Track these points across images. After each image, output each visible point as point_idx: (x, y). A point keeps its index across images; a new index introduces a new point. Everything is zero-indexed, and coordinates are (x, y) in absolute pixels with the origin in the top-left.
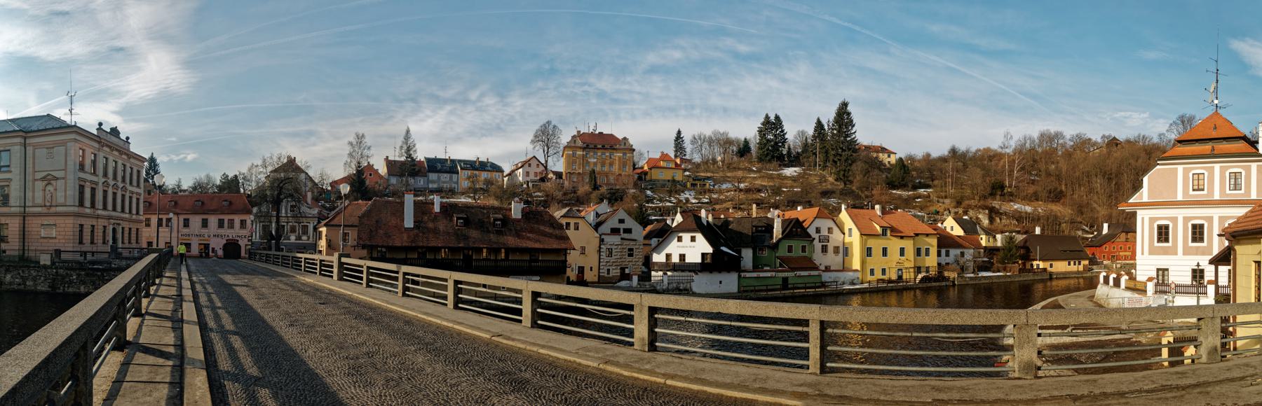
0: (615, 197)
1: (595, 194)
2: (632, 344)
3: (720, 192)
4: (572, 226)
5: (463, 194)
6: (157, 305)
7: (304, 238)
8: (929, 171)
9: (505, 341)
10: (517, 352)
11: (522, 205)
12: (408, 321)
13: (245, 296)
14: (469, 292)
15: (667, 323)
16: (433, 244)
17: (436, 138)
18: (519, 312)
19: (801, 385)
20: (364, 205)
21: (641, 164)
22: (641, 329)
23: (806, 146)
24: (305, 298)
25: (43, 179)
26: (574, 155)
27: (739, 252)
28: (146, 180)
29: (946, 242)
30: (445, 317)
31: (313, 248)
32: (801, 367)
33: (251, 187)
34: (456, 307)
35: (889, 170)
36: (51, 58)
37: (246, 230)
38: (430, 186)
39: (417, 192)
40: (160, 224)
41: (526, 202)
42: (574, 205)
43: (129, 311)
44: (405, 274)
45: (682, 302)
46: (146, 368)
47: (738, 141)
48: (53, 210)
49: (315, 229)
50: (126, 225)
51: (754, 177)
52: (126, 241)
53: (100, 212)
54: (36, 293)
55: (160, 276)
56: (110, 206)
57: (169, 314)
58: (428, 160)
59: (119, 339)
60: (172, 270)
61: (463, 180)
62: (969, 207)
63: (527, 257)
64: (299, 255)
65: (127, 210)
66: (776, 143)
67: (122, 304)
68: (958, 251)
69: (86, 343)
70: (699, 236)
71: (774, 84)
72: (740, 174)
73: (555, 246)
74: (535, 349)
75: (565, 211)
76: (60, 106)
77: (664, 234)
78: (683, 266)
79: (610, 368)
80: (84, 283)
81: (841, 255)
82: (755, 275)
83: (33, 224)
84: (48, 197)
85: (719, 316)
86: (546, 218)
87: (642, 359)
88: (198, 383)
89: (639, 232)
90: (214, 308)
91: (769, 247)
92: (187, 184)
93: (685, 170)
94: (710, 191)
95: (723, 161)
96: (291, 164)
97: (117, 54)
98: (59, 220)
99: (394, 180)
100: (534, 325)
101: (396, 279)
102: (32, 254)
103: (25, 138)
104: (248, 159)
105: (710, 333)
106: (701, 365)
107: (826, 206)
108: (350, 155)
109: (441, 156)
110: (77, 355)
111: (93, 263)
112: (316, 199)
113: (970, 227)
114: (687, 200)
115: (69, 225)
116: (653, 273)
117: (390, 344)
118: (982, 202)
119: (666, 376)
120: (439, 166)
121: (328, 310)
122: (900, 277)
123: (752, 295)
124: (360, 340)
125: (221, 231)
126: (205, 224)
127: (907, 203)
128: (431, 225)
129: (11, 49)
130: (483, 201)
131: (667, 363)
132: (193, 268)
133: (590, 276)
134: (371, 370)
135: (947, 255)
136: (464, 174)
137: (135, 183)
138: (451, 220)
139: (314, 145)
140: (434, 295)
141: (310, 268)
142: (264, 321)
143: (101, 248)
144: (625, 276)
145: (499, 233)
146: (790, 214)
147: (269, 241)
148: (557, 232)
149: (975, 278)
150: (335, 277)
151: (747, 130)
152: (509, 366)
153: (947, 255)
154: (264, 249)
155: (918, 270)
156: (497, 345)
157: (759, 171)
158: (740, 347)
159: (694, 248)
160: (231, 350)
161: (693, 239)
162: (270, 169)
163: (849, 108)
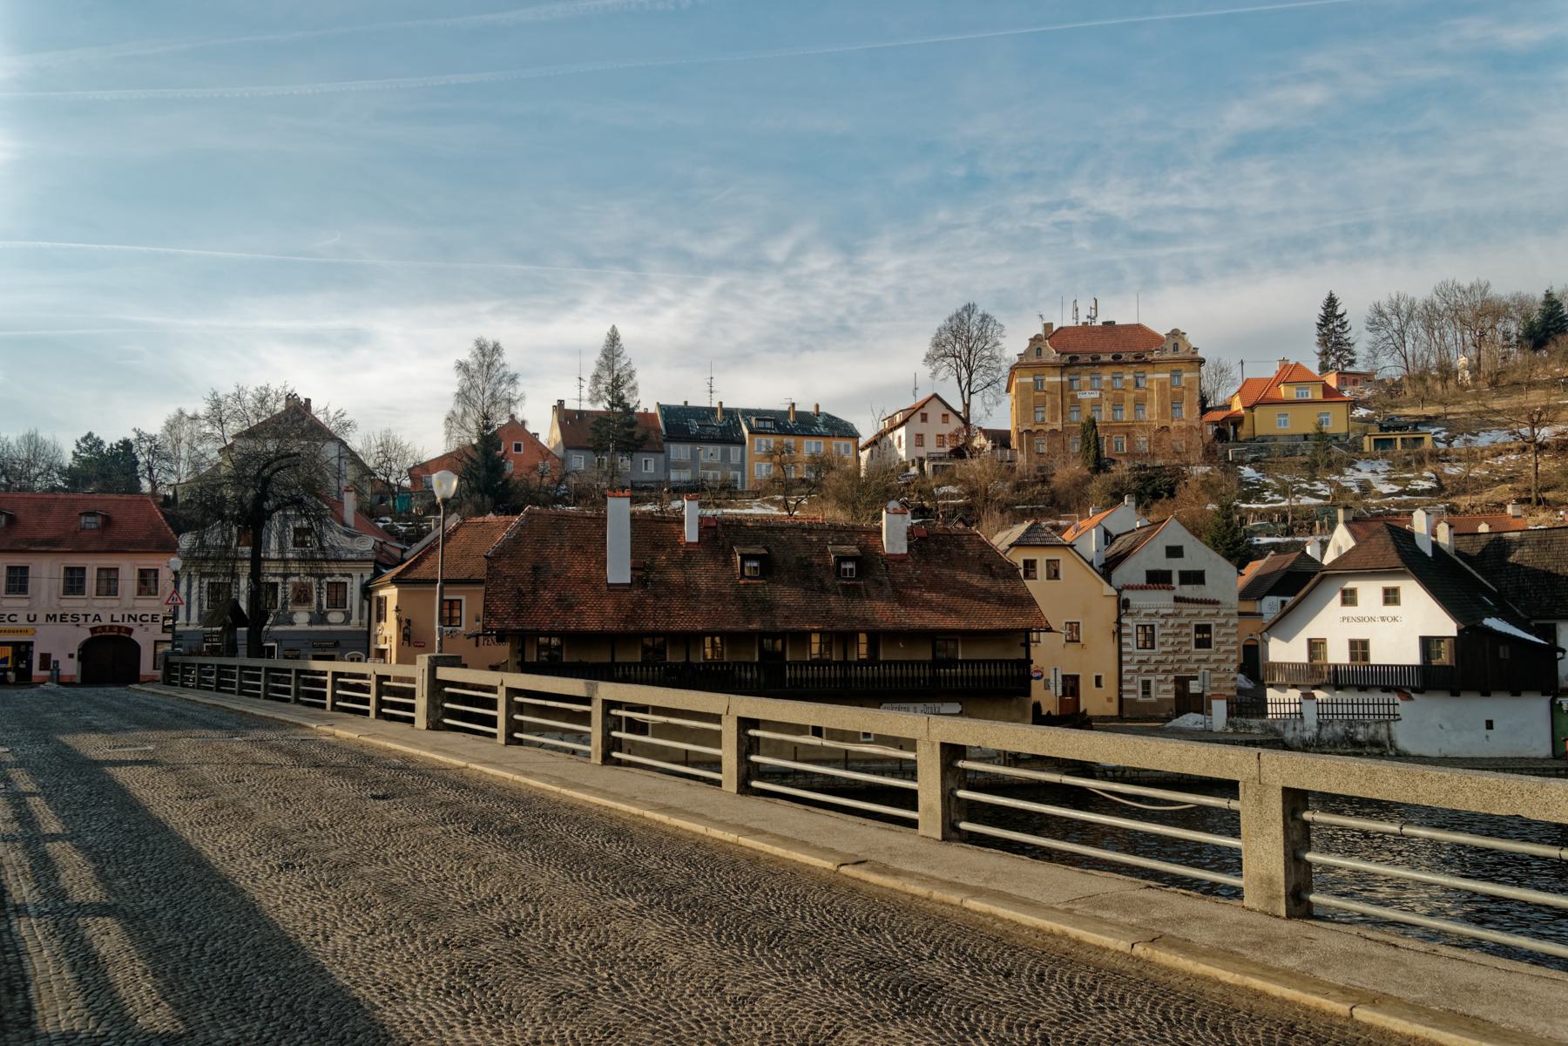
0: (1154, 488)
1: (1098, 484)
2: (1237, 893)
3: (1472, 457)
4: (1041, 569)
5: (756, 494)
9: (875, 879)
11: (908, 520)
12: (620, 831)
13: (144, 794)
14: (778, 749)
16: (682, 624)
17: (687, 355)
18: (909, 799)
20: (499, 527)
21: (1221, 398)
22: (1262, 851)
24: (333, 786)
26: (1038, 385)
27: (1549, 633)
30: (716, 817)
31: (362, 644)
33: (175, 477)
34: (744, 788)
37: (158, 600)
38: (674, 476)
39: (639, 492)
41: (920, 512)
44: (609, 705)
47: (1522, 304)
49: (367, 591)
58: (667, 411)
61: (756, 459)
63: (925, 654)
70: (1412, 591)
72: (1536, 398)
73: (998, 624)
74: (955, 898)
75: (1020, 529)
77: (1298, 583)
78: (1362, 675)
79: (1164, 957)
86: (972, 550)
89: (1226, 582)
93: (1354, 404)
94: (1436, 457)
95: (1475, 369)
99: (579, 461)
100: (951, 833)
101: (585, 718)
108: (463, 396)
109: (700, 400)
112: (369, 513)
114: (1366, 487)
116: (1271, 694)
117: (567, 897)
120: (694, 426)
121: (396, 813)
124: (485, 891)
125: (74, 604)
128: (675, 576)
130: (807, 511)
131: (1351, 958)
133: (1093, 701)
134: (512, 971)
136: (757, 446)
138: (728, 562)
140: (687, 759)
142: (200, 863)
144: (1187, 702)
145: (851, 592)
148: (1002, 586)
152: (886, 945)
154: (214, 651)
156: (854, 889)
159: (1399, 623)
161: (1391, 597)
162: (234, 427)
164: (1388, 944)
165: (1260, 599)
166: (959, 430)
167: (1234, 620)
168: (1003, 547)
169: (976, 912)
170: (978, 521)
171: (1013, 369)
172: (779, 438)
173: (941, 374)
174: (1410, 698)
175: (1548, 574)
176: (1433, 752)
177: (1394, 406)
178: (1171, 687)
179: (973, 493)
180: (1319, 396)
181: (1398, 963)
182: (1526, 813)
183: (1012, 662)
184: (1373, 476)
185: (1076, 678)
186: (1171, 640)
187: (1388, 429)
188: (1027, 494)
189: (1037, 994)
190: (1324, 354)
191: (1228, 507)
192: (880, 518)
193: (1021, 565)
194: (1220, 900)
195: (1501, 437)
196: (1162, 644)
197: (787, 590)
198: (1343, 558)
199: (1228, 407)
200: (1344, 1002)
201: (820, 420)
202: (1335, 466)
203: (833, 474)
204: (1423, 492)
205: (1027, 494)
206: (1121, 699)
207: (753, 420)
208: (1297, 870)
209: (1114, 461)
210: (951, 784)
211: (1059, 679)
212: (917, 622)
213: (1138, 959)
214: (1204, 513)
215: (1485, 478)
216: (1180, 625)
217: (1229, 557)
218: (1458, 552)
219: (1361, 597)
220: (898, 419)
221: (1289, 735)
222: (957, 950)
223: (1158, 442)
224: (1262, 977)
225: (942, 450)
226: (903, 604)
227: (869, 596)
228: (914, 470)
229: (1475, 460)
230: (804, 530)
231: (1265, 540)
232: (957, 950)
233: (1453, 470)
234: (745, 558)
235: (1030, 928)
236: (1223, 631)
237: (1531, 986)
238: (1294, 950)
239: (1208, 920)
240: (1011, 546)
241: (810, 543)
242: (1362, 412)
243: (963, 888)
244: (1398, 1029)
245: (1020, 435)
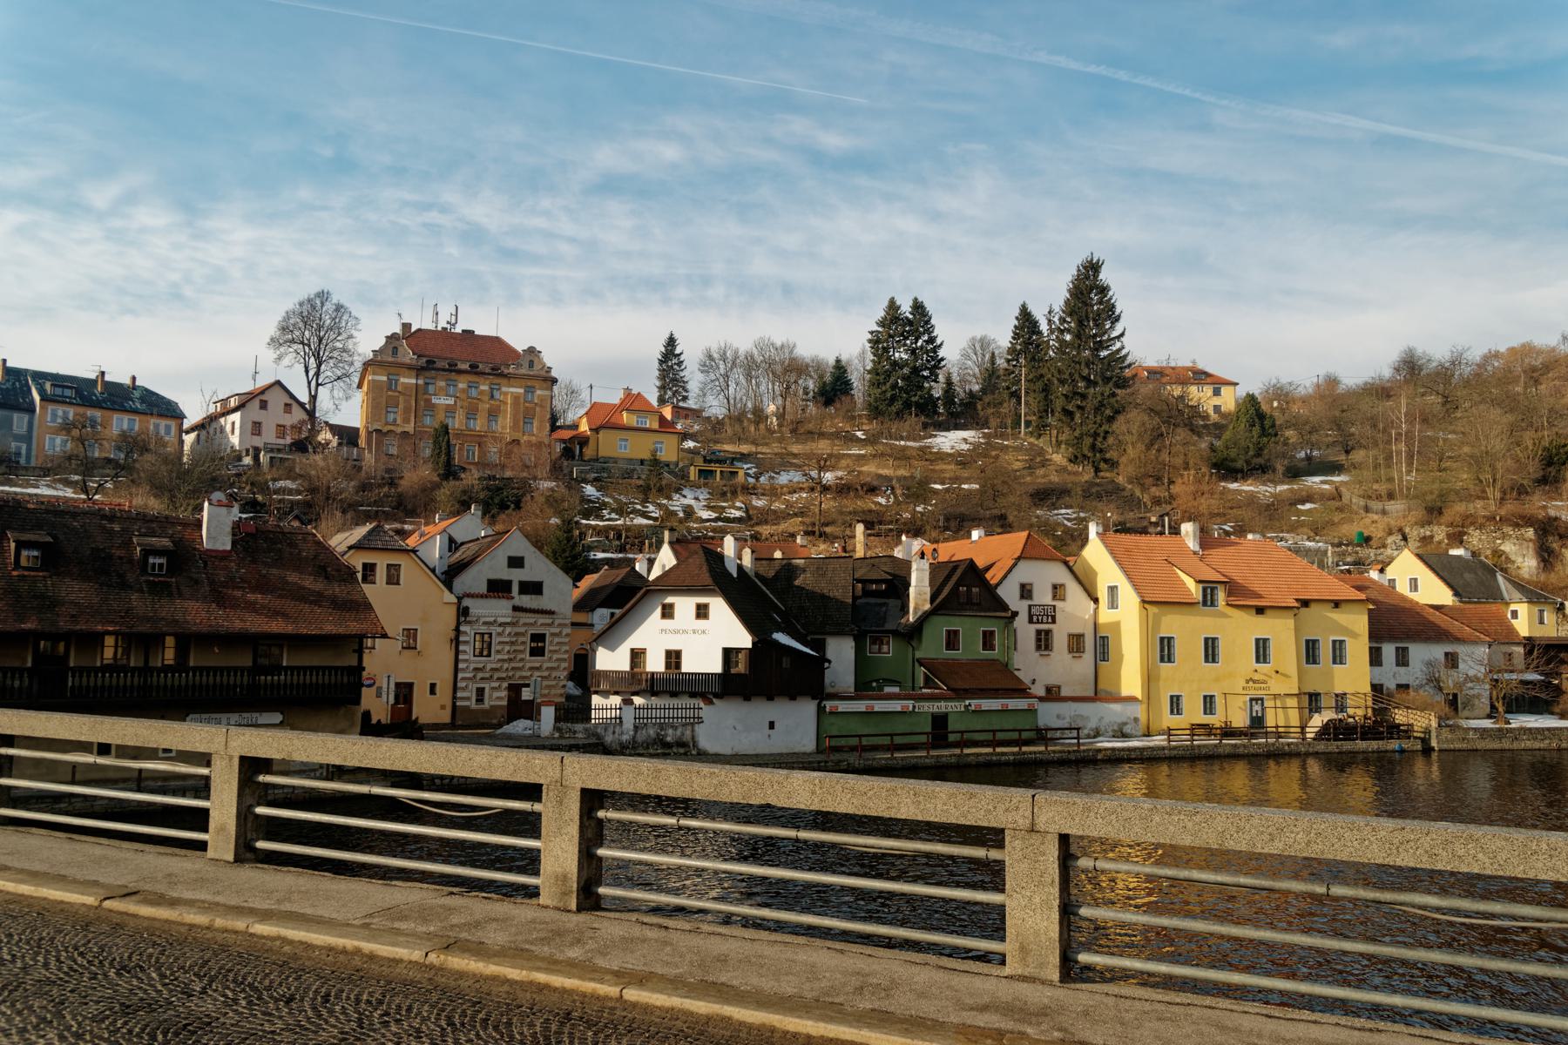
0: (500, 499)
1: (445, 492)
4: (381, 574)
5: (45, 472)
8: (1337, 424)
9: (146, 911)
10: (187, 937)
11: (235, 513)
15: (630, 835)
18: (199, 819)
19: (984, 1008)
21: (571, 417)
22: (559, 851)
23: (991, 375)
26: (391, 384)
27: (820, 646)
29: (1395, 624)
32: (984, 957)
35: (1218, 428)
41: (251, 505)
42: (389, 517)
45: (671, 778)
47: (818, 366)
51: (859, 454)
62: (1469, 520)
63: (246, 660)
66: (916, 371)
68: (1437, 652)
70: (719, 606)
71: (910, 224)
72: (823, 447)
73: (329, 629)
74: (240, 925)
75: (361, 532)
77: (626, 598)
78: (674, 682)
79: (457, 962)
81: (1089, 655)
82: (861, 706)
85: (767, 814)
86: (307, 551)
87: (559, 933)
89: (562, 592)
91: (895, 633)
93: (685, 436)
94: (748, 490)
95: (781, 415)
100: (246, 853)
105: (743, 859)
106: (717, 946)
107: (1048, 529)
113: (1475, 581)
114: (689, 512)
116: (596, 700)
118: (1510, 507)
119: (623, 977)
122: (1257, 722)
123: (853, 759)
127: (1272, 516)
130: (109, 495)
131: (627, 943)
133: (427, 709)
135: (1402, 659)
136: (49, 416)
144: (520, 708)
145: (159, 589)
146: (953, 550)
148: (337, 589)
149: (1500, 734)
151: (842, 339)
152: (152, 984)
153: (1402, 659)
155: (1313, 701)
156: (118, 924)
157: (871, 440)
158: (819, 898)
159: (705, 635)
161: (702, 612)
163: (1105, 276)
164: (660, 926)
165: (593, 610)
166: (303, 422)
167: (568, 630)
168: (342, 548)
169: (263, 937)
170: (318, 518)
171: (367, 365)
172: (81, 410)
173: (286, 361)
174: (711, 703)
175: (823, 596)
176: (727, 751)
177: (716, 442)
178: (504, 694)
179: (313, 490)
180: (656, 426)
181: (666, 943)
182: (773, 801)
183: (343, 668)
184: (693, 501)
185: (410, 686)
186: (507, 648)
187: (710, 461)
188: (372, 496)
189: (320, 1016)
190: (663, 388)
191: (569, 522)
192: (202, 510)
193: (360, 568)
194: (519, 900)
195: (794, 476)
196: (498, 652)
197: (76, 585)
198: (666, 574)
199: (575, 426)
200: (616, 984)
201: (137, 394)
202: (666, 491)
203: (148, 457)
204: (734, 520)
205: (372, 496)
206: (454, 706)
207: (48, 386)
208: (589, 866)
209: (464, 469)
210: (249, 801)
211: (392, 686)
212: (238, 625)
213: (431, 967)
214: (546, 526)
215: (782, 512)
216: (517, 634)
217: (566, 570)
218: (757, 575)
219: (677, 611)
220: (233, 403)
221: (609, 738)
222: (234, 981)
223: (509, 454)
224: (548, 971)
225: (281, 441)
226: (221, 605)
227: (181, 595)
228: (247, 460)
229: (776, 495)
230: (104, 517)
231: (600, 555)
232: (234, 981)
233: (759, 503)
234: (20, 545)
235: (321, 948)
236: (557, 640)
237: (768, 951)
238: (579, 941)
239: (503, 921)
240: (350, 548)
241: (111, 532)
242: (690, 444)
243: (252, 912)
244: (658, 1003)
245: (369, 433)
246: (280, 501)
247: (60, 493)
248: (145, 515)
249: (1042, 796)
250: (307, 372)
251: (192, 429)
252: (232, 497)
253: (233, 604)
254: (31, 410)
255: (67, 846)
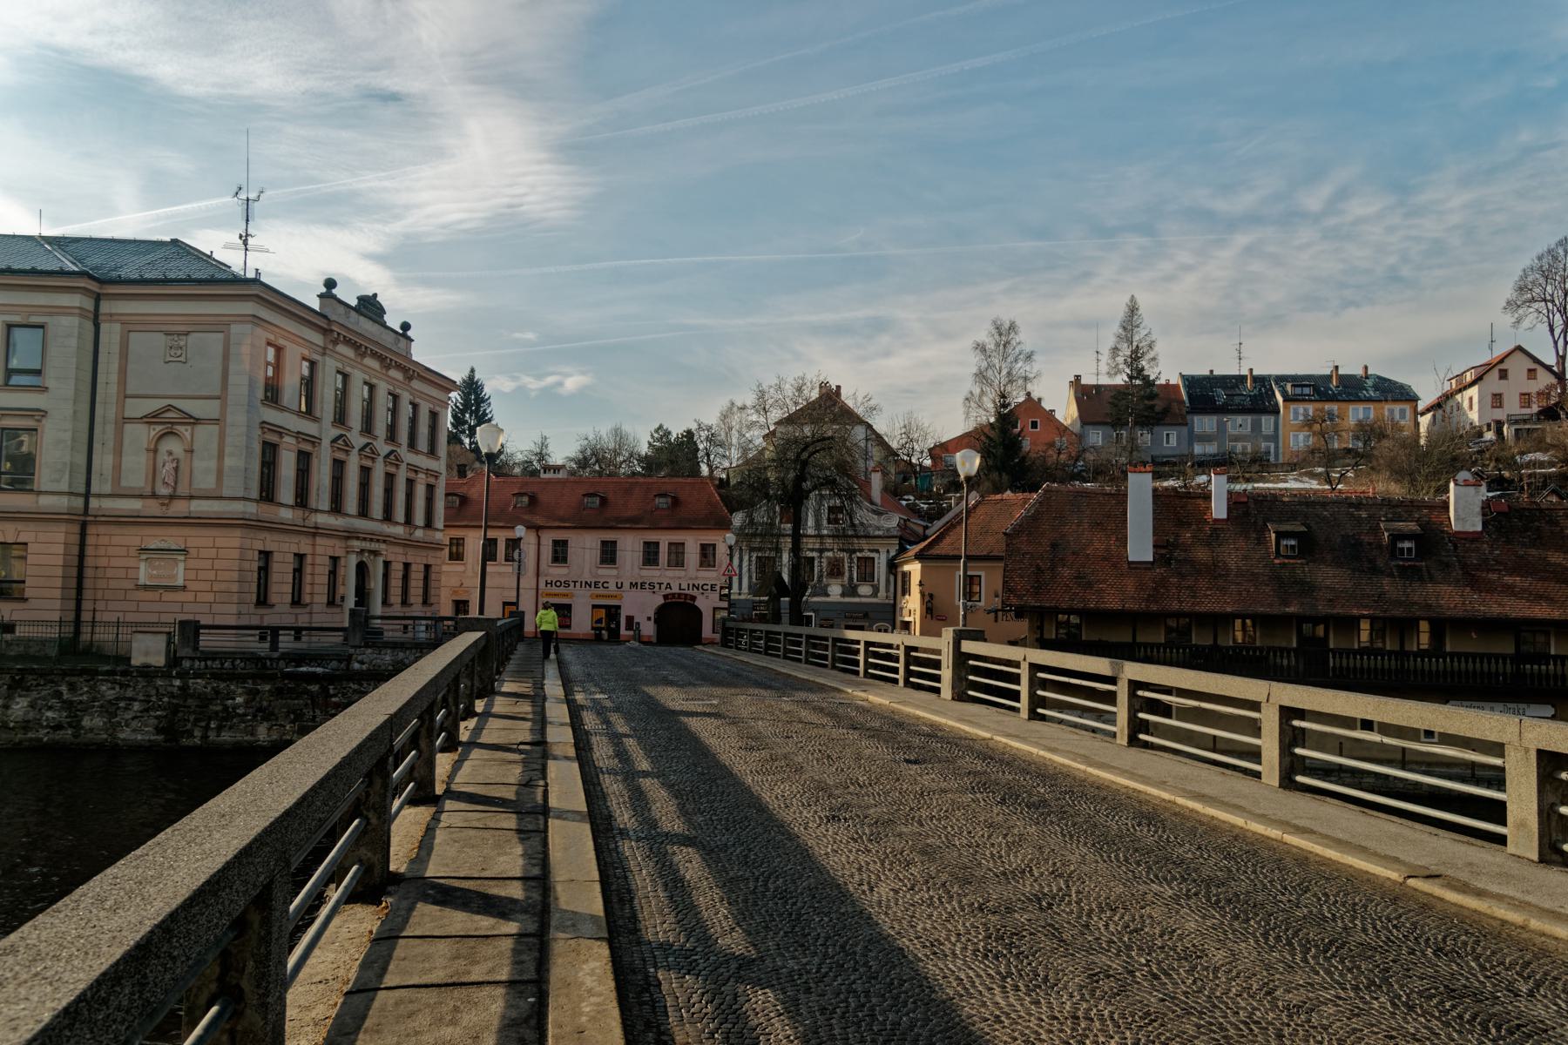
5: (1292, 467)
6: (478, 771)
7: (865, 590)
9: (1452, 896)
10: (1500, 933)
11: (1484, 493)
12: (1150, 815)
13: (712, 742)
14: (1322, 742)
18: (1497, 812)
20: (1017, 504)
24: (868, 748)
25: (151, 418)
28: (454, 439)
30: (1254, 808)
31: (888, 616)
33: (727, 462)
36: (188, 90)
37: (715, 571)
39: (1161, 467)
40: (489, 553)
41: (1497, 483)
43: (398, 791)
44: (1135, 685)
46: (443, 947)
48: (179, 508)
49: (893, 566)
50: (397, 556)
52: (395, 597)
53: (323, 519)
54: (113, 752)
55: (488, 691)
56: (351, 503)
57: (509, 794)
58: (1191, 382)
59: (367, 870)
60: (520, 675)
61: (1292, 429)
63: (1508, 648)
64: (852, 635)
65: (400, 515)
67: (380, 769)
69: (268, 888)
76: (212, 221)
80: (267, 715)
83: (114, 551)
84: (166, 471)
88: (585, 979)
90: (630, 775)
92: (562, 452)
96: (829, 403)
97: (381, 108)
98: (197, 539)
99: (1096, 437)
100: (1287, 782)
102: (104, 636)
103: (98, 298)
104: (724, 399)
108: (981, 376)
109: (1226, 367)
110: (240, 925)
111: (299, 658)
112: (894, 491)
115: (228, 554)
117: (1100, 878)
120: (1221, 396)
121: (929, 778)
124: (1016, 861)
125: (651, 574)
126: (609, 554)
128: (1202, 554)
129: (64, 38)
130: (1352, 484)
132: (575, 670)
134: (1047, 944)
136: (1292, 415)
137: (423, 444)
138: (1261, 540)
139: (887, 354)
141: (881, 667)
142: (762, 808)
143: (322, 616)
145: (1410, 574)
147: (775, 599)
150: (947, 693)
154: (762, 619)
156: (1427, 905)
160: (675, 886)
162: (776, 415)
166: (1551, 387)
172: (1319, 405)
173: (1526, 323)
197: (1331, 571)
201: (1370, 383)
203: (1386, 443)
207: (1289, 387)
210: (1551, 798)
212: (1495, 610)
220: (1469, 377)
225: (1527, 411)
227: (1432, 579)
228: (1489, 436)
230: (1351, 505)
234: (1281, 535)
246: (1530, 476)
247: (1307, 486)
248: (1390, 501)
249: (1527, 721)
250: (1552, 330)
251: (1428, 410)
252: (1479, 476)
253: (1490, 588)
254: (1276, 411)
255: (1362, 818)
